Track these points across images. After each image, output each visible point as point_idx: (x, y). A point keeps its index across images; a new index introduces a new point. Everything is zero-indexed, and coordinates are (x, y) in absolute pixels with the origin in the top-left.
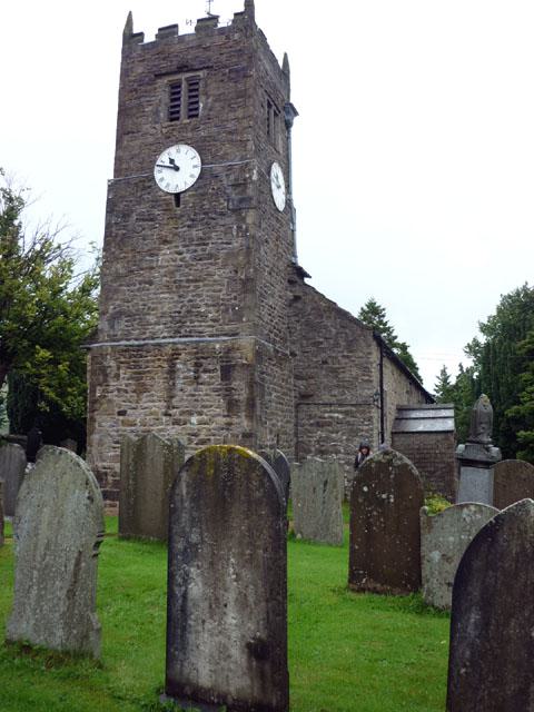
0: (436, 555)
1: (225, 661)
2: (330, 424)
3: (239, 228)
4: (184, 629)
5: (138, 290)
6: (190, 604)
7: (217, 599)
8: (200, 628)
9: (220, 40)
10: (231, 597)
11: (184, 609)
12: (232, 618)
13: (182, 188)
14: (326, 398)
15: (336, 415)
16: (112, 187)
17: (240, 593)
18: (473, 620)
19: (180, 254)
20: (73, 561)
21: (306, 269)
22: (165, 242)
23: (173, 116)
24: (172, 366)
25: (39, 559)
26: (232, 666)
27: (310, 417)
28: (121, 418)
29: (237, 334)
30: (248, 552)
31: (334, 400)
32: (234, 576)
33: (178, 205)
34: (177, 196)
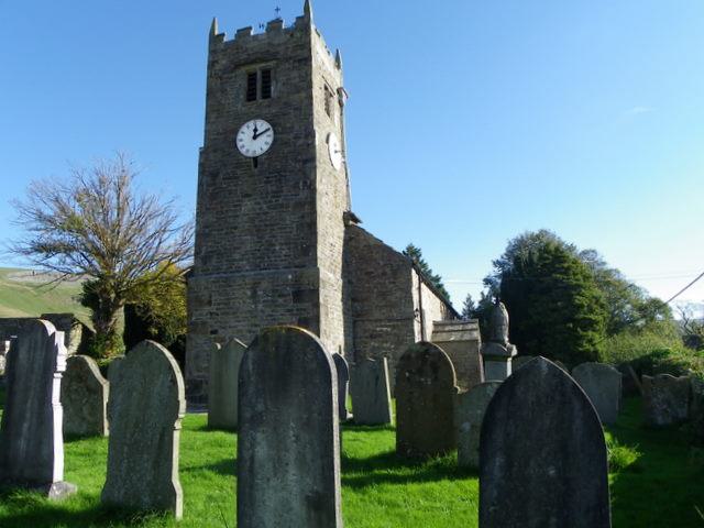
0: (467, 426)
1: (287, 513)
2: (380, 336)
3: (305, 183)
4: (251, 487)
5: (226, 233)
6: (257, 465)
7: (279, 458)
8: (265, 486)
9: (283, 38)
10: (291, 457)
11: (251, 470)
12: (292, 474)
13: (259, 153)
14: (377, 315)
15: (385, 329)
16: (204, 153)
17: (299, 452)
18: (498, 464)
19: (259, 203)
20: (158, 436)
21: (357, 215)
22: (247, 195)
23: (251, 96)
24: (254, 293)
25: (128, 436)
26: (294, 517)
27: (365, 331)
28: (213, 336)
29: (304, 266)
30: (305, 416)
31: (383, 317)
32: (293, 438)
33: (256, 166)
34: (255, 159)
